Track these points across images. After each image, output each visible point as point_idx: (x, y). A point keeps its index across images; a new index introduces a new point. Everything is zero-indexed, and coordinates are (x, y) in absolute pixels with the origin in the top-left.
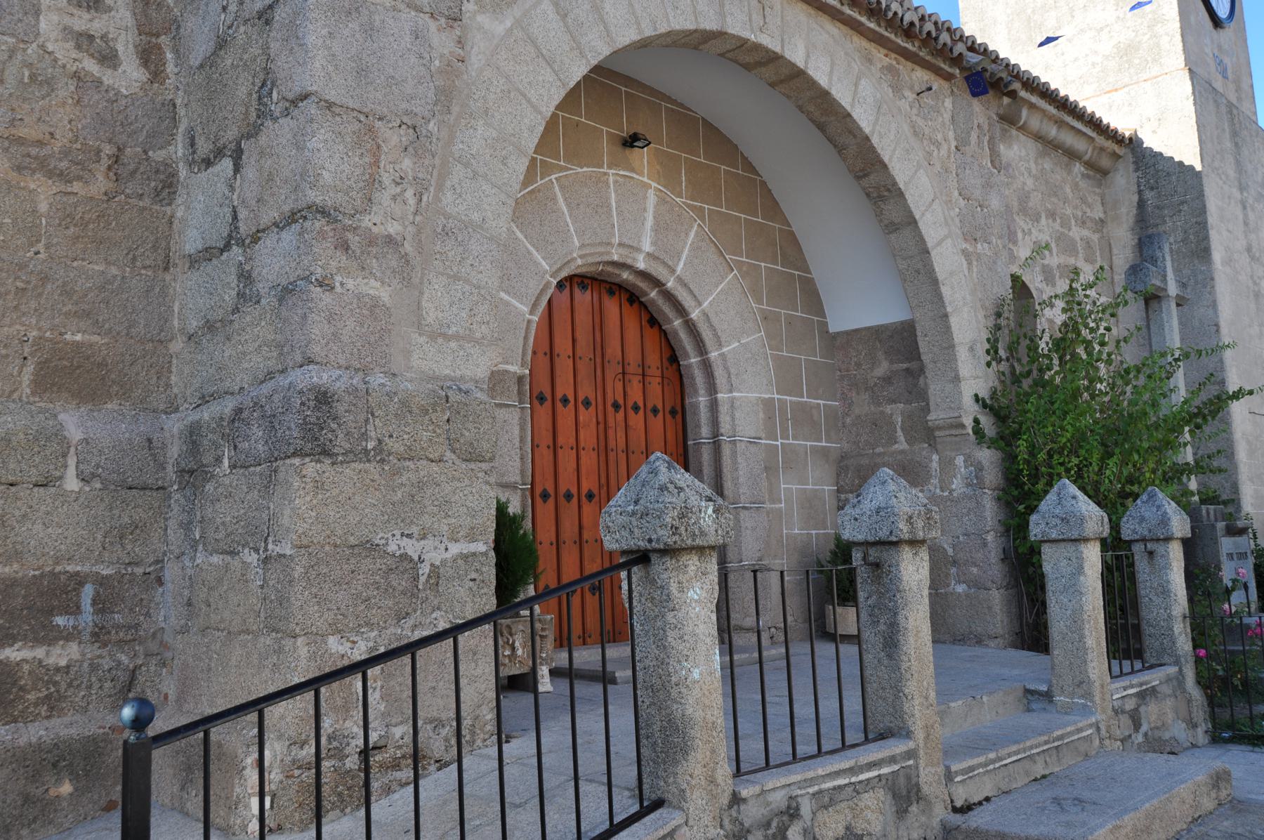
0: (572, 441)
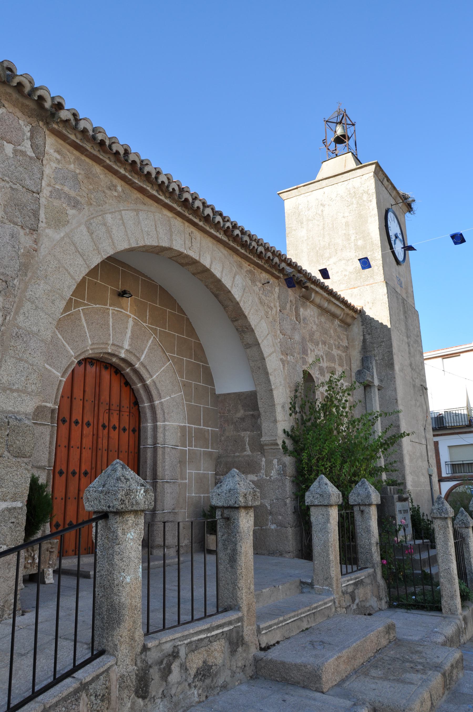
0: (79, 444)
